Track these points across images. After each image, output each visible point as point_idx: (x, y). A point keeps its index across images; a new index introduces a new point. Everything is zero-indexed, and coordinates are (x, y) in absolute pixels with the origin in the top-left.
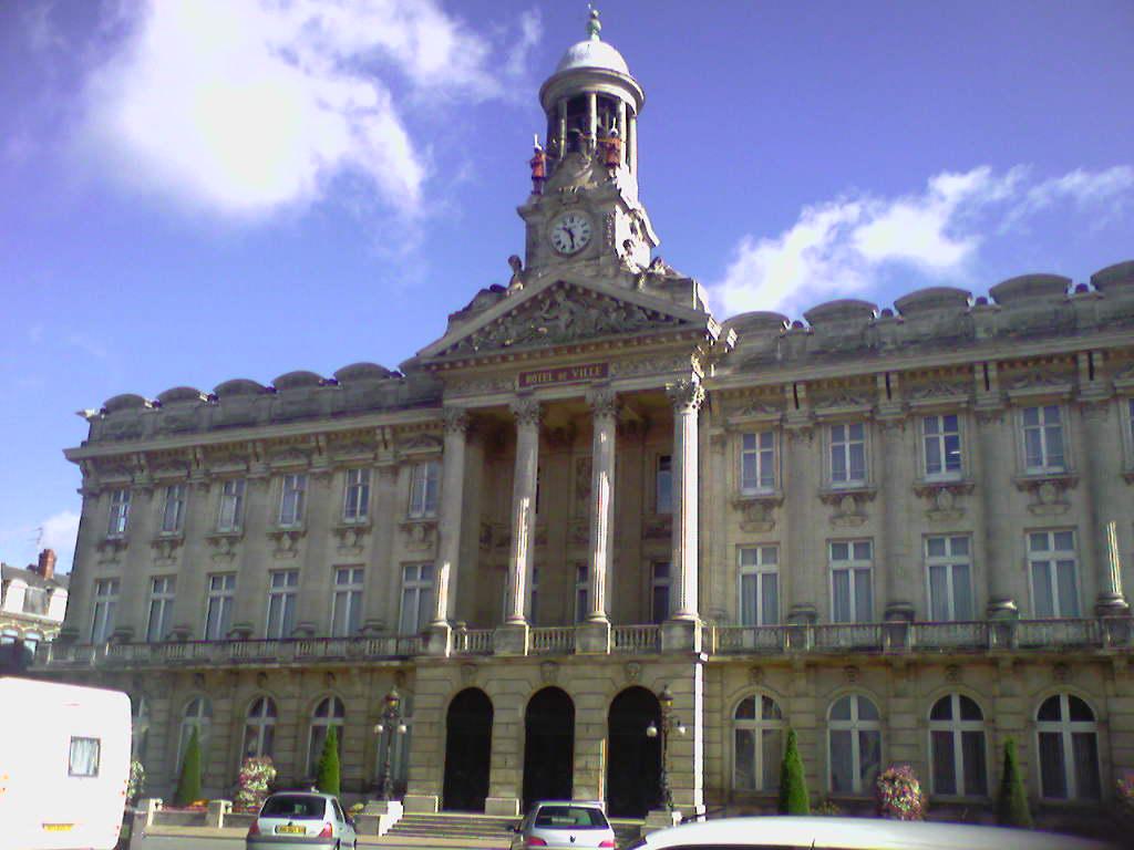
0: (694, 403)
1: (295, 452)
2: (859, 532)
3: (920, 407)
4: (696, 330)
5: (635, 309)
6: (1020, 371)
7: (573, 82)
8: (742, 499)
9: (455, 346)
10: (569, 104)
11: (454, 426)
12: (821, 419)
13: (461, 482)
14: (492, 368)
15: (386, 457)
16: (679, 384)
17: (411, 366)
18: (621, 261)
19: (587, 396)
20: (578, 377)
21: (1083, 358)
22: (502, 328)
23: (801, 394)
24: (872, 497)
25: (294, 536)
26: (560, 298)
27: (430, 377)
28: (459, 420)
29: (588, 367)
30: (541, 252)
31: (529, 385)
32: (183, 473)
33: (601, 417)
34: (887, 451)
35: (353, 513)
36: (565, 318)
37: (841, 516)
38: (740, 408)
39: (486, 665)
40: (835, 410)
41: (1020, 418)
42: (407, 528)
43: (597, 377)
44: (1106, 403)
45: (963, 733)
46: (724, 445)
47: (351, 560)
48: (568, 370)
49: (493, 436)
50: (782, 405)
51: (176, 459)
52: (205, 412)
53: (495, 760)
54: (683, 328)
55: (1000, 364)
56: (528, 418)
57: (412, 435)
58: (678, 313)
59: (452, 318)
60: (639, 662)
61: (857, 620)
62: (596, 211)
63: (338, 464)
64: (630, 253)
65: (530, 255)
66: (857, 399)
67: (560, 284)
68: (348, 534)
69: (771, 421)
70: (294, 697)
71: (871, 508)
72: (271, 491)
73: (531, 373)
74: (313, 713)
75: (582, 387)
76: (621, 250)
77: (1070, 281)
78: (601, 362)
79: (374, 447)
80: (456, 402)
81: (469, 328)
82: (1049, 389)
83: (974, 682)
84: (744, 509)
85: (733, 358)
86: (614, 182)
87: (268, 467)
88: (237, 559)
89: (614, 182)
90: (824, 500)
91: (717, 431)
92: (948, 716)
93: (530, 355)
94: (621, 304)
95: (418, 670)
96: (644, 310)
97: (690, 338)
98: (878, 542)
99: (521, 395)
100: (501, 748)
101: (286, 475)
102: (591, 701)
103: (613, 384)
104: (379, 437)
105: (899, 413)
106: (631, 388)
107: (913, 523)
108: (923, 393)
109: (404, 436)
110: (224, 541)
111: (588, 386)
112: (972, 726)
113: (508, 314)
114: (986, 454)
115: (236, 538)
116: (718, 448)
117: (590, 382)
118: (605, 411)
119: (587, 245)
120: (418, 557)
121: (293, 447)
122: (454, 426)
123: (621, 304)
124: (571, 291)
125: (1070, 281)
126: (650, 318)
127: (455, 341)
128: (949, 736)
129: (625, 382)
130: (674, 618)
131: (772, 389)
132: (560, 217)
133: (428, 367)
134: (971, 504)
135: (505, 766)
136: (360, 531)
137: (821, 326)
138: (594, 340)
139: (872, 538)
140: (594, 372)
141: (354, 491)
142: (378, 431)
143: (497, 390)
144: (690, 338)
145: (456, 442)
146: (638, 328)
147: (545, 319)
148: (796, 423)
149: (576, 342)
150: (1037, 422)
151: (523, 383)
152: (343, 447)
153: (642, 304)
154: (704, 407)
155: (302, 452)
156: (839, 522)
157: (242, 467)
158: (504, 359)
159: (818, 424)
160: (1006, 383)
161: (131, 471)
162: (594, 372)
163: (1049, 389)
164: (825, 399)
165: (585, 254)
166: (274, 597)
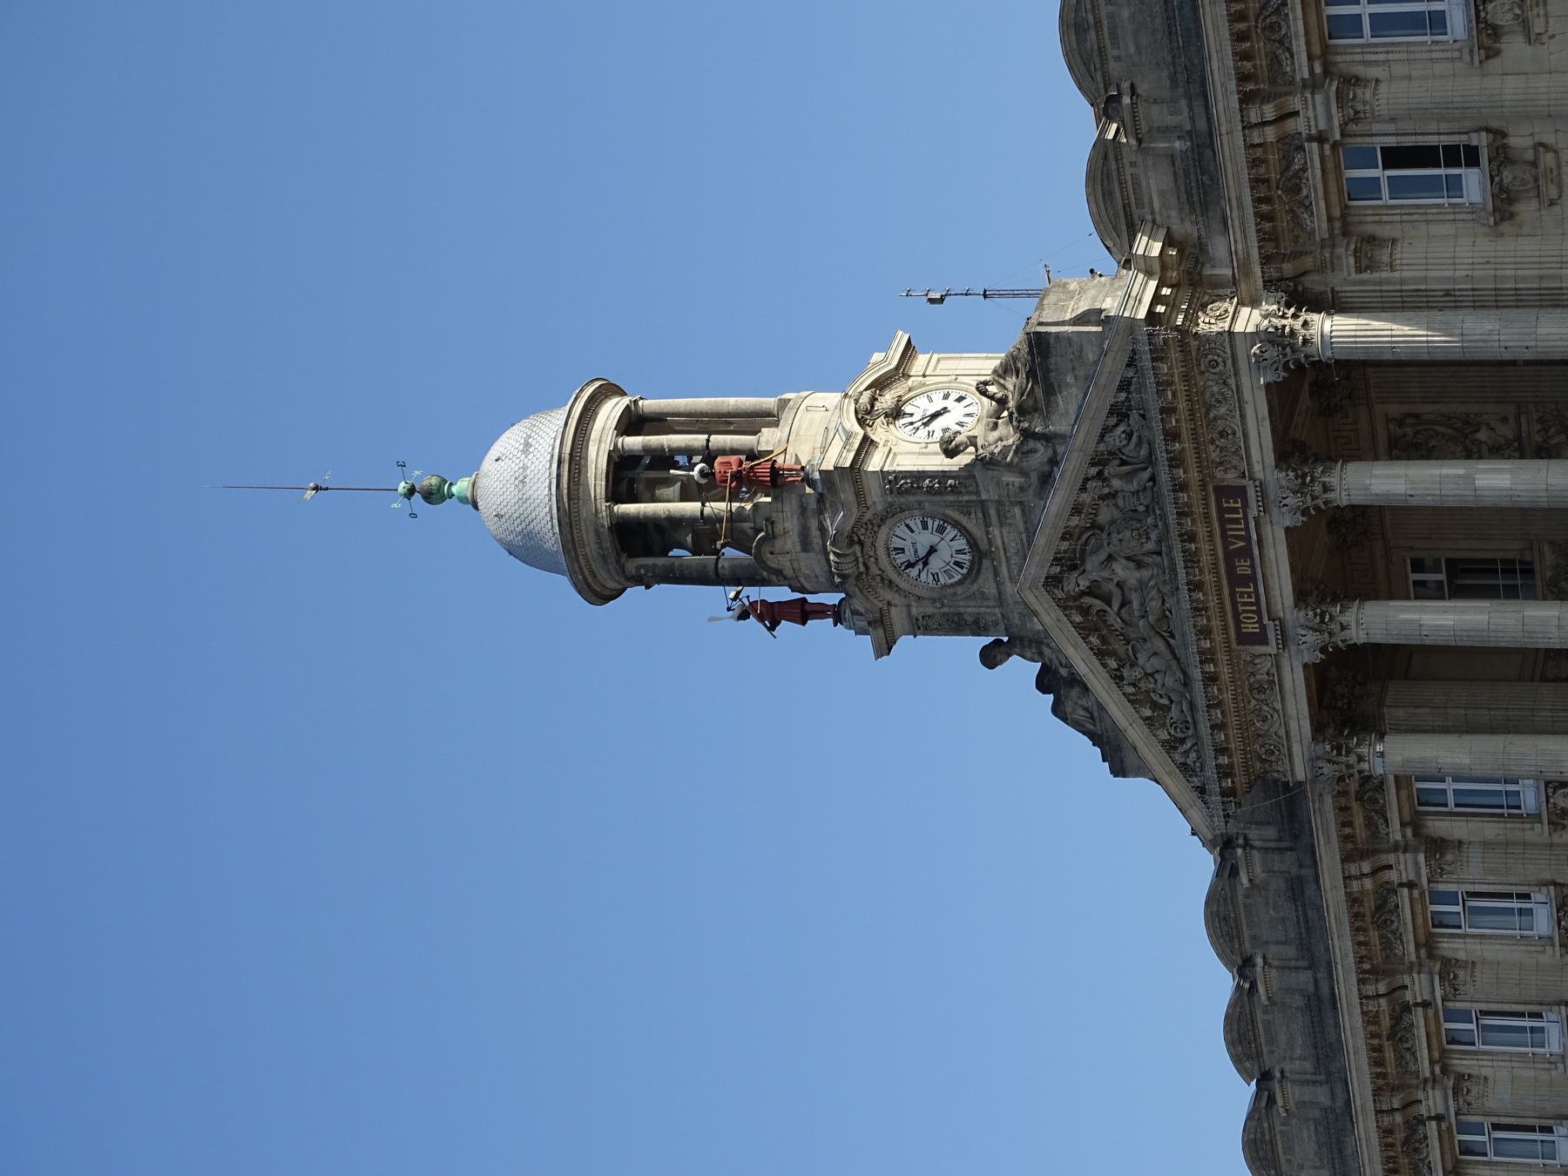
0: (1298, 324)
1: (1399, 1032)
7: (591, 549)
8: (1490, 207)
9: (1185, 768)
11: (1352, 759)
12: (1318, 69)
13: (1468, 740)
15: (1408, 866)
16: (1260, 359)
18: (985, 463)
20: (1248, 538)
26: (1076, 583)
29: (1223, 522)
31: (1263, 628)
33: (1330, 496)
36: (1121, 570)
37: (1525, 25)
40: (1299, 46)
43: (1245, 505)
46: (1372, 240)
48: (1229, 557)
49: (1356, 690)
56: (1335, 627)
57: (1359, 820)
58: (1113, 367)
59: (1119, 770)
62: (880, 507)
63: (1423, 952)
64: (972, 441)
65: (977, 629)
72: (1486, 1072)
73: (1238, 622)
75: (1267, 530)
76: (964, 459)
78: (1213, 499)
79: (1388, 890)
81: (1136, 734)
84: (1511, 201)
85: (1185, 228)
86: (817, 476)
89: (817, 476)
90: (1492, 53)
94: (1094, 471)
96: (1106, 430)
103: (1259, 475)
105: (1327, 98)
108: (1284, 56)
109: (1360, 831)
111: (1265, 519)
116: (1384, 256)
117: (1257, 520)
118: (1318, 488)
119: (957, 525)
121: (1392, 1032)
122: (1352, 759)
123: (1094, 471)
124: (1069, 562)
131: (1254, 163)
138: (1172, 519)
140: (1235, 510)
142: (1355, 886)
143: (1275, 682)
145: (1394, 753)
147: (1122, 605)
148: (1330, 118)
151: (1261, 639)
152: (1387, 946)
153: (1095, 436)
154: (1302, 299)
155: (1396, 1020)
156: (1538, 27)
157: (1418, 1016)
159: (1445, 1070)
162: (1235, 510)
164: (1275, 61)
165: (978, 532)
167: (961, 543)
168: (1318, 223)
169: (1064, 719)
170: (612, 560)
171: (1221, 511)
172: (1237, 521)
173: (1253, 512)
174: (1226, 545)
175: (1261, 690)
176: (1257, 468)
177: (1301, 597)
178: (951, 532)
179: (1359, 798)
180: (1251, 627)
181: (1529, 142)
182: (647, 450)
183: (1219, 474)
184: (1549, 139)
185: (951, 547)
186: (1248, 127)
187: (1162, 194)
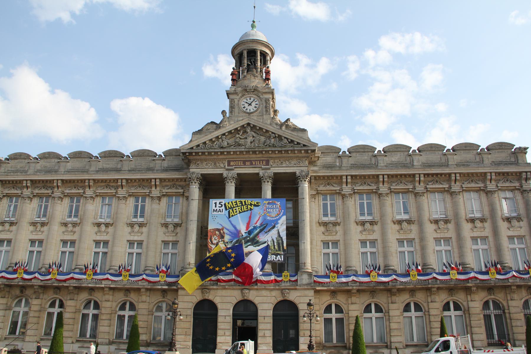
2: (371, 237)
3: (394, 189)
4: (311, 150)
5: (283, 138)
6: (430, 178)
10: (247, 53)
11: (195, 181)
14: (215, 157)
17: (169, 153)
19: (260, 173)
20: (255, 165)
21: (381, 177)
22: (220, 140)
23: (349, 180)
24: (339, 224)
25: (107, 225)
27: (184, 158)
28: (197, 178)
29: (260, 161)
30: (236, 110)
31: (232, 166)
32: (49, 191)
34: (382, 206)
35: (136, 216)
36: (250, 139)
37: (365, 230)
38: (322, 184)
39: (214, 289)
40: (361, 188)
41: (321, 197)
42: (166, 225)
44: (350, 194)
45: (336, 319)
47: (136, 238)
48: (251, 161)
50: (484, 181)
51: (46, 184)
52: (416, 158)
53: (219, 332)
54: (305, 148)
55: (425, 175)
59: (194, 133)
60: (288, 289)
61: (135, 273)
66: (371, 184)
67: (249, 124)
68: (135, 226)
69: (336, 190)
70: (109, 301)
71: (144, 230)
74: (118, 309)
75: (258, 169)
77: (376, 148)
80: (197, 170)
81: (206, 138)
82: (441, 186)
83: (341, 300)
87: (95, 192)
88: (143, 235)
91: (314, 193)
92: (330, 312)
93: (235, 153)
94: (277, 136)
95: (179, 291)
96: (287, 139)
97: (308, 153)
98: (379, 241)
99: (227, 170)
100: (222, 327)
101: (103, 196)
102: (266, 306)
103: (271, 169)
104: (55, 184)
106: (209, 172)
107: (393, 234)
110: (70, 225)
111: (260, 169)
112: (339, 316)
113: (224, 134)
114: (419, 209)
115: (76, 224)
119: (256, 111)
120: (171, 239)
123: (277, 136)
125: (376, 148)
126: (289, 143)
127: (198, 144)
128: (331, 320)
129: (276, 168)
130: (303, 270)
132: (244, 97)
133: (184, 154)
134: (414, 228)
135: (224, 335)
136: (141, 225)
137: (168, 158)
139: (143, 241)
140: (263, 163)
141: (136, 207)
144: (308, 153)
146: (285, 146)
147: (240, 138)
149: (257, 150)
150: (73, 202)
151: (229, 165)
158: (222, 153)
160: (497, 181)
161: (22, 188)
162: (263, 163)
163: (441, 186)
165: (255, 114)
166: (62, 252)
167: (252, 111)
168: (321, 188)
169: (207, 125)
170: (248, 48)
171: (263, 160)
172: (260, 163)
173: (263, 166)
174: (254, 161)
175: (215, 164)
176: (274, 169)
177: (238, 174)
178: (255, 109)
179: (174, 184)
180: (232, 163)
181: (338, 230)
182: (258, 60)
183: (272, 161)
184: (338, 234)
185: (251, 108)
186: (347, 176)
187: (326, 160)
